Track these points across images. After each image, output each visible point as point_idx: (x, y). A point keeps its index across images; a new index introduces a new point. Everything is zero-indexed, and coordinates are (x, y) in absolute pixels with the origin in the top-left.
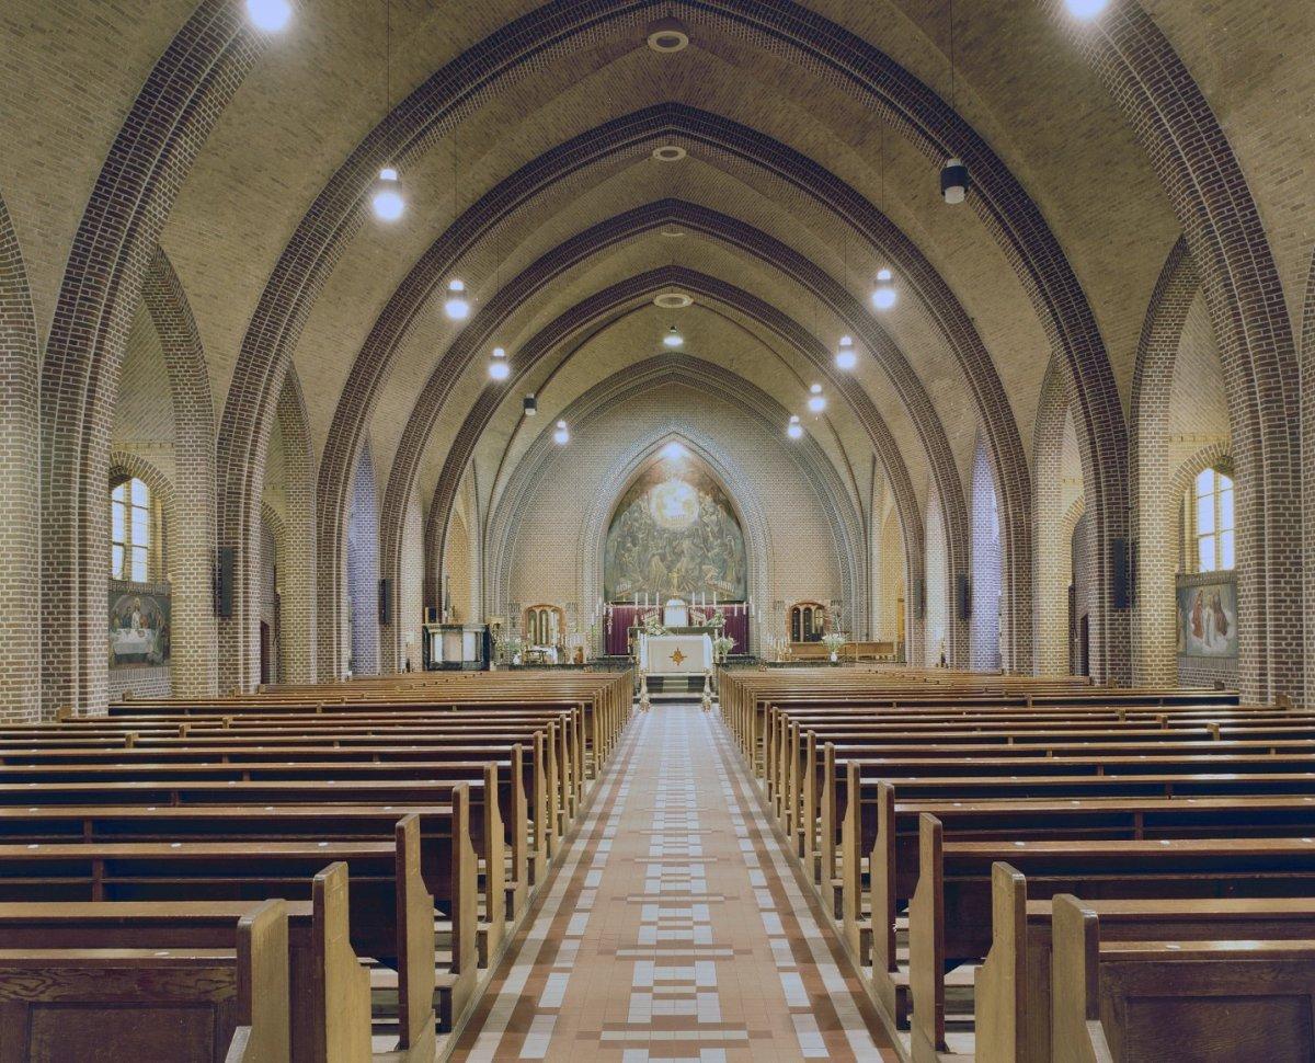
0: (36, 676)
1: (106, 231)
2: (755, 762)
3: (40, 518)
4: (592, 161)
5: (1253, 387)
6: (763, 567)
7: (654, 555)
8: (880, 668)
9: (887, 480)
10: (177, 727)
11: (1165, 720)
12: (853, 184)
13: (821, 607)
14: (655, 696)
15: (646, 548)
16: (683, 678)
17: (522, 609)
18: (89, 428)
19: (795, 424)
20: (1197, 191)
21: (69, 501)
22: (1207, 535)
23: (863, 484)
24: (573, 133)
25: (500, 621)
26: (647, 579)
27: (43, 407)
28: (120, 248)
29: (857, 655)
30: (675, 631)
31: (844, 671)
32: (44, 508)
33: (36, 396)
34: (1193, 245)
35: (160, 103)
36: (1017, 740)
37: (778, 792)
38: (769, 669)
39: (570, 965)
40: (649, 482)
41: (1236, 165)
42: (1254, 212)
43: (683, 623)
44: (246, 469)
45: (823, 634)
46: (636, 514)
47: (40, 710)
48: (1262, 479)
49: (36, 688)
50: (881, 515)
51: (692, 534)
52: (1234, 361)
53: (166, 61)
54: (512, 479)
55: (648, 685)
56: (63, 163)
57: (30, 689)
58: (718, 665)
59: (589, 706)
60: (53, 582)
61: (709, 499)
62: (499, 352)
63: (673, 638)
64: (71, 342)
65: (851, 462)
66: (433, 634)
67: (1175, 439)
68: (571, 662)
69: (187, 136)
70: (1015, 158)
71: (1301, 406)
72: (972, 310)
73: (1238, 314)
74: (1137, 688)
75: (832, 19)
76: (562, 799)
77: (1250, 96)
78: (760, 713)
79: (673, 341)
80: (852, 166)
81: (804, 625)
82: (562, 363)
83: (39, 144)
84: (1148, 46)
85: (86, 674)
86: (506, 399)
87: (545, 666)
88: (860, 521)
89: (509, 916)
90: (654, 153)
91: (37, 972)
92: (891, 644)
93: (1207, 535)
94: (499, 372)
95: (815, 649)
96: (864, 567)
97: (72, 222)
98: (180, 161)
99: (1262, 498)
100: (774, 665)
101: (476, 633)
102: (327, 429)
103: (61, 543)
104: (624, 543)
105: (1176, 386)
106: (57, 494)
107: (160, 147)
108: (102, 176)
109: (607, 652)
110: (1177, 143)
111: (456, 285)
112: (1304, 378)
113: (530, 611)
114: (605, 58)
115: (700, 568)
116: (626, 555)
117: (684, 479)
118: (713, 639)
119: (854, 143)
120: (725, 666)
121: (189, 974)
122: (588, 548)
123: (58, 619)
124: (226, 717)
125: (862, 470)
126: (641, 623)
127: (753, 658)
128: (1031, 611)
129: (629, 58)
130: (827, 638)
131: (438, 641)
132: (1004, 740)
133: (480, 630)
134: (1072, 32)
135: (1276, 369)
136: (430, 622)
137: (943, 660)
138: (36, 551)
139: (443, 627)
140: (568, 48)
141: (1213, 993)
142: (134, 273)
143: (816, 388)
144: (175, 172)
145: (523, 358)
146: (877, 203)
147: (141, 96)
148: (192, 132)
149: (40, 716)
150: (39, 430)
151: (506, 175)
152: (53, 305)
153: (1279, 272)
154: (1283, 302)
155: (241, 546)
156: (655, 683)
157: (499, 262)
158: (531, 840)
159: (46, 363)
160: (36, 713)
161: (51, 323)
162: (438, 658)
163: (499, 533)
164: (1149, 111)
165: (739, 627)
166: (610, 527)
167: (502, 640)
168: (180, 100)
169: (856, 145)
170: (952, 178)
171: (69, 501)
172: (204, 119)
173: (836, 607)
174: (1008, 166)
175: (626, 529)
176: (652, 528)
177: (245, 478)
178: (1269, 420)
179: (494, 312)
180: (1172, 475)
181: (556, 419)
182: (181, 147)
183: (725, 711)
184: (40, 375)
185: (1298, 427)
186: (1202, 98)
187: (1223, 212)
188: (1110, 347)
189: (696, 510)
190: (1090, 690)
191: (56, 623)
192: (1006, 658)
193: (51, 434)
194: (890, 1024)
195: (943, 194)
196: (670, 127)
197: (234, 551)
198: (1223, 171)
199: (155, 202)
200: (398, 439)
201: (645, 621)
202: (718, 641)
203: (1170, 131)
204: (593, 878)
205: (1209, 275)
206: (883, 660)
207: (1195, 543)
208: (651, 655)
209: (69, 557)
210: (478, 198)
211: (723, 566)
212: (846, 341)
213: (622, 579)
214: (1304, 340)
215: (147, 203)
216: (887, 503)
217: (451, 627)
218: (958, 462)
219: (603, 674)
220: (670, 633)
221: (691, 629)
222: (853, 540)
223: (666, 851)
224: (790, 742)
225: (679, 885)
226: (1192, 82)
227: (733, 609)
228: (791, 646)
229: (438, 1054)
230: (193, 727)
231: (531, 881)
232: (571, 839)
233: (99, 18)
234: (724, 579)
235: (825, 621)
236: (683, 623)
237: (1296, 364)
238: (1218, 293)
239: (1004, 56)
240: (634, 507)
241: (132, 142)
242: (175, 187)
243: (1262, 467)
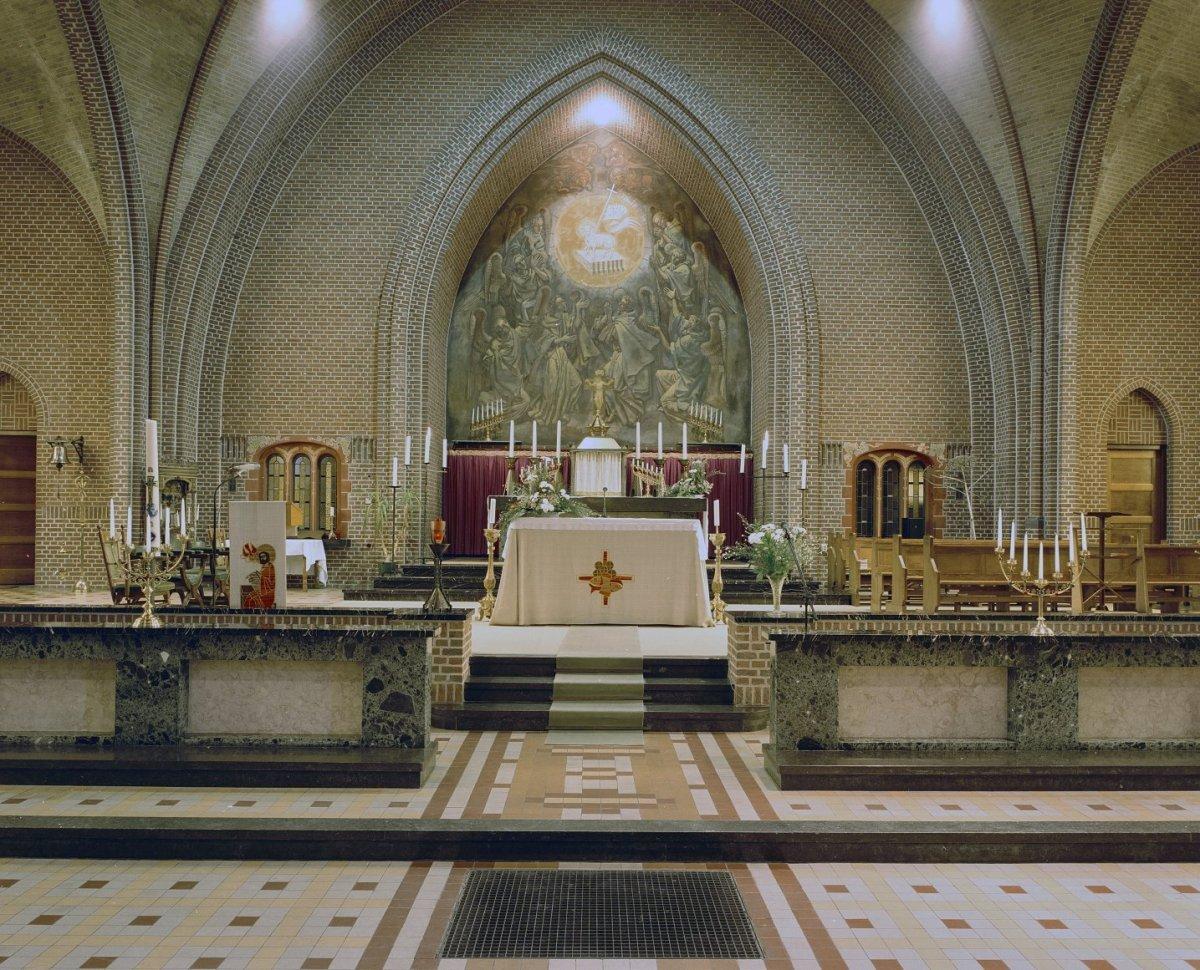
7: (553, 346)
13: (922, 461)
15: (537, 332)
17: (848, 458)
26: (538, 395)
43: (616, 490)
46: (518, 258)
51: (636, 303)
61: (672, 229)
63: (589, 522)
65: (1017, 119)
104: (492, 320)
116: (496, 344)
117: (622, 187)
122: (403, 314)
166: (463, 284)
175: (495, 289)
176: (552, 290)
189: (645, 252)
211: (700, 372)
213: (485, 396)
220: (582, 508)
225: (602, 782)
234: (701, 398)
236: (616, 490)
240: (514, 242)
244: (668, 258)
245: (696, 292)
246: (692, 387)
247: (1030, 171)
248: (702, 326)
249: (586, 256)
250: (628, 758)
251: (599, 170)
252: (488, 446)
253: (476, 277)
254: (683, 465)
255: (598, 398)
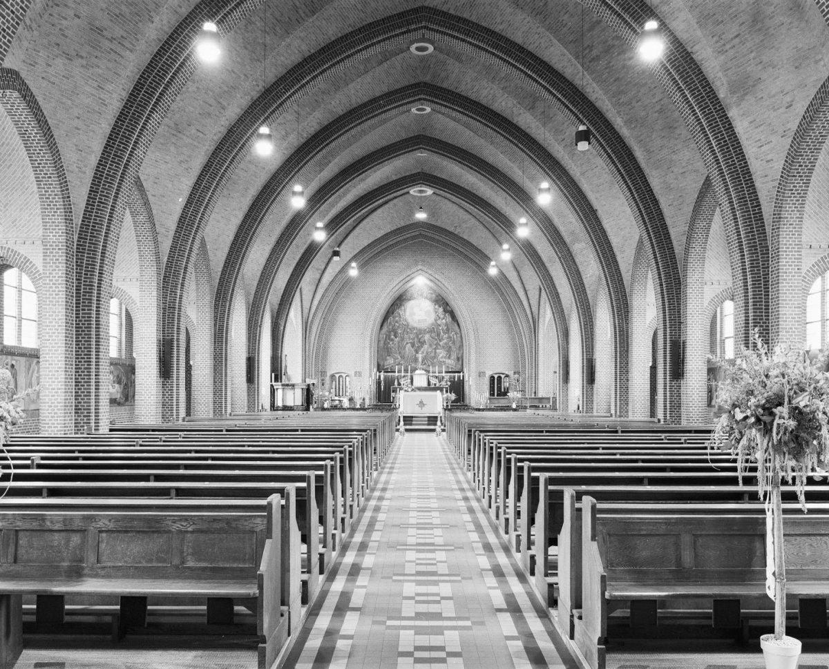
0: (72, 410)
1: (112, 165)
2: (466, 462)
3: (74, 322)
4: (375, 116)
5: (744, 259)
6: (473, 351)
8: (541, 412)
9: (548, 305)
10: (28, 458)
11: (685, 440)
12: (528, 131)
13: (507, 376)
14: (408, 427)
15: (403, 339)
16: (424, 417)
17: (487, 376)
18: (102, 273)
19: (493, 266)
20: (714, 150)
21: (90, 314)
22: (730, 337)
23: (534, 302)
24: (366, 99)
25: (315, 381)
27: (77, 262)
28: (120, 174)
29: (528, 405)
30: (420, 389)
31: (520, 414)
32: (76, 317)
33: (73, 256)
34: (713, 179)
35: (143, 95)
36: (603, 448)
37: (478, 477)
38: (476, 412)
39: (375, 552)
40: (405, 299)
41: (736, 136)
42: (746, 162)
43: (425, 384)
44: (178, 294)
45: (508, 392)
47: (73, 428)
48: (748, 309)
49: (72, 416)
50: (544, 321)
51: (431, 331)
52: (734, 244)
53: (147, 71)
54: (323, 296)
55: (404, 421)
56: (90, 128)
57: (69, 417)
58: (445, 410)
59: (375, 430)
60: (82, 358)
61: (441, 310)
62: (320, 225)
63: (418, 393)
64: (92, 226)
65: (527, 289)
66: (277, 389)
67: (708, 283)
68: (358, 406)
69: (157, 112)
70: (618, 122)
71: (770, 270)
72: (596, 204)
73: (737, 218)
74: (684, 424)
75: (516, 41)
76: (363, 479)
77: (744, 99)
78: (470, 436)
79: (421, 216)
80: (526, 120)
81: (497, 387)
82: (354, 228)
83: (78, 118)
84: (688, 70)
85: (98, 409)
86: (322, 249)
87: (342, 409)
88: (532, 326)
89: (343, 531)
90: (412, 110)
91: (186, 520)
92: (549, 399)
93: (730, 337)
94: (320, 236)
95: (503, 401)
96: (534, 351)
97: (93, 160)
98: (153, 126)
99: (748, 320)
100: (479, 410)
101: (302, 389)
102: (220, 270)
103: (86, 337)
104: (390, 336)
105: (709, 253)
106: (84, 310)
107: (142, 119)
108: (110, 135)
109: (379, 400)
110: (704, 123)
111: (298, 188)
112: (772, 254)
113: (333, 376)
114: (386, 57)
115: (435, 352)
117: (426, 298)
118: (443, 394)
119: (528, 108)
120: (450, 410)
121: (246, 520)
123: (84, 379)
124: (179, 433)
125: (533, 295)
126: (399, 384)
127: (467, 406)
128: (628, 380)
129: (399, 57)
130: (510, 394)
131: (279, 394)
132: (598, 448)
133: (304, 387)
134: (666, 34)
135: (757, 249)
136: (275, 382)
137: (578, 408)
138: (72, 341)
139: (283, 385)
140: (365, 54)
141: (642, 533)
142: (127, 188)
143: (506, 246)
144: (150, 132)
145: (332, 226)
146: (541, 142)
147: (132, 91)
148: (160, 110)
149: (73, 432)
150: (75, 274)
151: (326, 123)
152: (83, 205)
153: (760, 195)
154: (761, 212)
155: (175, 338)
156: (408, 420)
157: (321, 171)
158: (351, 499)
159: (79, 237)
160: (72, 430)
161: (82, 215)
162: (279, 403)
163: (314, 329)
164: (689, 106)
165: (458, 388)
166: (382, 326)
167: (317, 393)
168: (154, 93)
169: (529, 110)
170: (583, 136)
171: (90, 314)
172: (166, 103)
173: (517, 376)
174: (615, 127)
175: (391, 327)
177: (178, 299)
178: (752, 277)
179: (318, 198)
180: (706, 304)
181: (350, 261)
182: (154, 118)
183: (449, 437)
184: (75, 244)
185: (768, 281)
186: (718, 99)
187: (729, 162)
188: (672, 231)
190: (658, 425)
191: (83, 381)
192: (613, 407)
193: (81, 276)
194: (528, 575)
195: (576, 145)
196: (422, 96)
197: (172, 341)
198: (729, 140)
199: (139, 148)
200: (259, 274)
201: (402, 383)
202: (445, 395)
203: (700, 117)
204: (381, 516)
205: (721, 196)
206: (544, 408)
207: (723, 342)
208: (405, 402)
209: (90, 345)
210: (310, 136)
211: (449, 350)
212: (523, 220)
213: (388, 358)
214: (772, 233)
215: (135, 150)
216: (547, 316)
217: (288, 385)
218: (588, 292)
219: (378, 413)
221: (430, 388)
222: (527, 335)
223: (418, 505)
224: (485, 449)
225: (428, 567)
226: (713, 90)
227: (454, 377)
228: (490, 399)
229: (320, 582)
230: (43, 458)
231: (351, 517)
232: (368, 499)
233: (111, 49)
234: (449, 358)
235: (510, 384)
237: (768, 246)
238: (726, 206)
239: (613, 66)
240: (396, 314)
241: (128, 116)
242: (149, 140)
243: (748, 303)
244: (439, 318)
245: (447, 328)
246: (447, 354)
247: (531, 302)
248: (450, 337)
249: (416, 318)
250: (449, 584)
251: (420, 293)
252: (390, 372)
253: (385, 324)
254: (443, 377)
255: (420, 360)
